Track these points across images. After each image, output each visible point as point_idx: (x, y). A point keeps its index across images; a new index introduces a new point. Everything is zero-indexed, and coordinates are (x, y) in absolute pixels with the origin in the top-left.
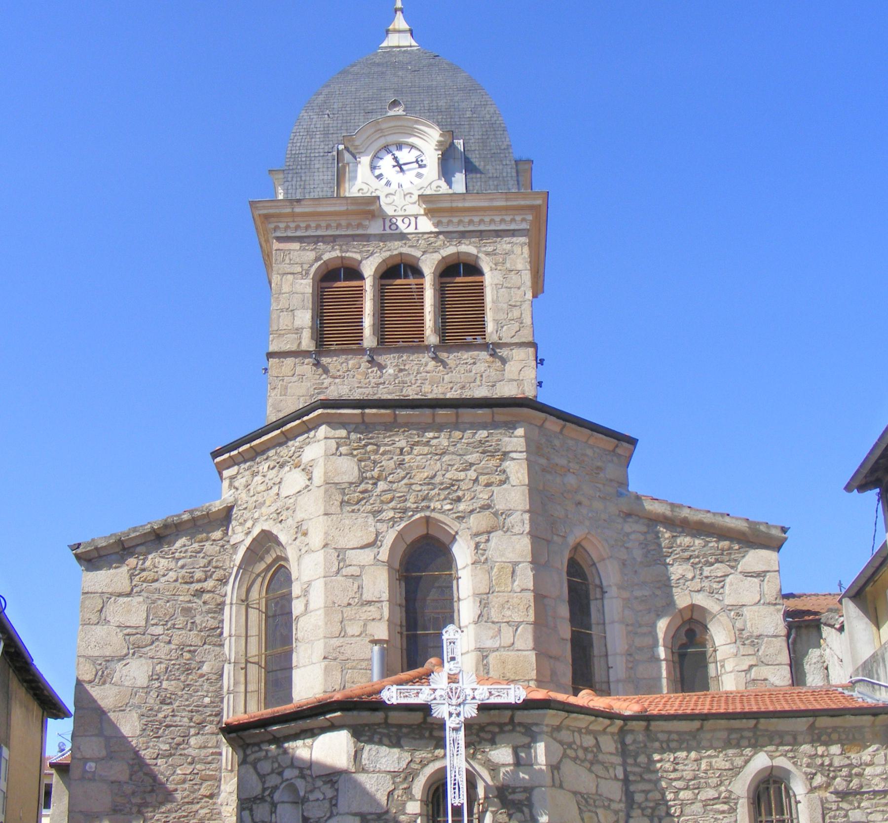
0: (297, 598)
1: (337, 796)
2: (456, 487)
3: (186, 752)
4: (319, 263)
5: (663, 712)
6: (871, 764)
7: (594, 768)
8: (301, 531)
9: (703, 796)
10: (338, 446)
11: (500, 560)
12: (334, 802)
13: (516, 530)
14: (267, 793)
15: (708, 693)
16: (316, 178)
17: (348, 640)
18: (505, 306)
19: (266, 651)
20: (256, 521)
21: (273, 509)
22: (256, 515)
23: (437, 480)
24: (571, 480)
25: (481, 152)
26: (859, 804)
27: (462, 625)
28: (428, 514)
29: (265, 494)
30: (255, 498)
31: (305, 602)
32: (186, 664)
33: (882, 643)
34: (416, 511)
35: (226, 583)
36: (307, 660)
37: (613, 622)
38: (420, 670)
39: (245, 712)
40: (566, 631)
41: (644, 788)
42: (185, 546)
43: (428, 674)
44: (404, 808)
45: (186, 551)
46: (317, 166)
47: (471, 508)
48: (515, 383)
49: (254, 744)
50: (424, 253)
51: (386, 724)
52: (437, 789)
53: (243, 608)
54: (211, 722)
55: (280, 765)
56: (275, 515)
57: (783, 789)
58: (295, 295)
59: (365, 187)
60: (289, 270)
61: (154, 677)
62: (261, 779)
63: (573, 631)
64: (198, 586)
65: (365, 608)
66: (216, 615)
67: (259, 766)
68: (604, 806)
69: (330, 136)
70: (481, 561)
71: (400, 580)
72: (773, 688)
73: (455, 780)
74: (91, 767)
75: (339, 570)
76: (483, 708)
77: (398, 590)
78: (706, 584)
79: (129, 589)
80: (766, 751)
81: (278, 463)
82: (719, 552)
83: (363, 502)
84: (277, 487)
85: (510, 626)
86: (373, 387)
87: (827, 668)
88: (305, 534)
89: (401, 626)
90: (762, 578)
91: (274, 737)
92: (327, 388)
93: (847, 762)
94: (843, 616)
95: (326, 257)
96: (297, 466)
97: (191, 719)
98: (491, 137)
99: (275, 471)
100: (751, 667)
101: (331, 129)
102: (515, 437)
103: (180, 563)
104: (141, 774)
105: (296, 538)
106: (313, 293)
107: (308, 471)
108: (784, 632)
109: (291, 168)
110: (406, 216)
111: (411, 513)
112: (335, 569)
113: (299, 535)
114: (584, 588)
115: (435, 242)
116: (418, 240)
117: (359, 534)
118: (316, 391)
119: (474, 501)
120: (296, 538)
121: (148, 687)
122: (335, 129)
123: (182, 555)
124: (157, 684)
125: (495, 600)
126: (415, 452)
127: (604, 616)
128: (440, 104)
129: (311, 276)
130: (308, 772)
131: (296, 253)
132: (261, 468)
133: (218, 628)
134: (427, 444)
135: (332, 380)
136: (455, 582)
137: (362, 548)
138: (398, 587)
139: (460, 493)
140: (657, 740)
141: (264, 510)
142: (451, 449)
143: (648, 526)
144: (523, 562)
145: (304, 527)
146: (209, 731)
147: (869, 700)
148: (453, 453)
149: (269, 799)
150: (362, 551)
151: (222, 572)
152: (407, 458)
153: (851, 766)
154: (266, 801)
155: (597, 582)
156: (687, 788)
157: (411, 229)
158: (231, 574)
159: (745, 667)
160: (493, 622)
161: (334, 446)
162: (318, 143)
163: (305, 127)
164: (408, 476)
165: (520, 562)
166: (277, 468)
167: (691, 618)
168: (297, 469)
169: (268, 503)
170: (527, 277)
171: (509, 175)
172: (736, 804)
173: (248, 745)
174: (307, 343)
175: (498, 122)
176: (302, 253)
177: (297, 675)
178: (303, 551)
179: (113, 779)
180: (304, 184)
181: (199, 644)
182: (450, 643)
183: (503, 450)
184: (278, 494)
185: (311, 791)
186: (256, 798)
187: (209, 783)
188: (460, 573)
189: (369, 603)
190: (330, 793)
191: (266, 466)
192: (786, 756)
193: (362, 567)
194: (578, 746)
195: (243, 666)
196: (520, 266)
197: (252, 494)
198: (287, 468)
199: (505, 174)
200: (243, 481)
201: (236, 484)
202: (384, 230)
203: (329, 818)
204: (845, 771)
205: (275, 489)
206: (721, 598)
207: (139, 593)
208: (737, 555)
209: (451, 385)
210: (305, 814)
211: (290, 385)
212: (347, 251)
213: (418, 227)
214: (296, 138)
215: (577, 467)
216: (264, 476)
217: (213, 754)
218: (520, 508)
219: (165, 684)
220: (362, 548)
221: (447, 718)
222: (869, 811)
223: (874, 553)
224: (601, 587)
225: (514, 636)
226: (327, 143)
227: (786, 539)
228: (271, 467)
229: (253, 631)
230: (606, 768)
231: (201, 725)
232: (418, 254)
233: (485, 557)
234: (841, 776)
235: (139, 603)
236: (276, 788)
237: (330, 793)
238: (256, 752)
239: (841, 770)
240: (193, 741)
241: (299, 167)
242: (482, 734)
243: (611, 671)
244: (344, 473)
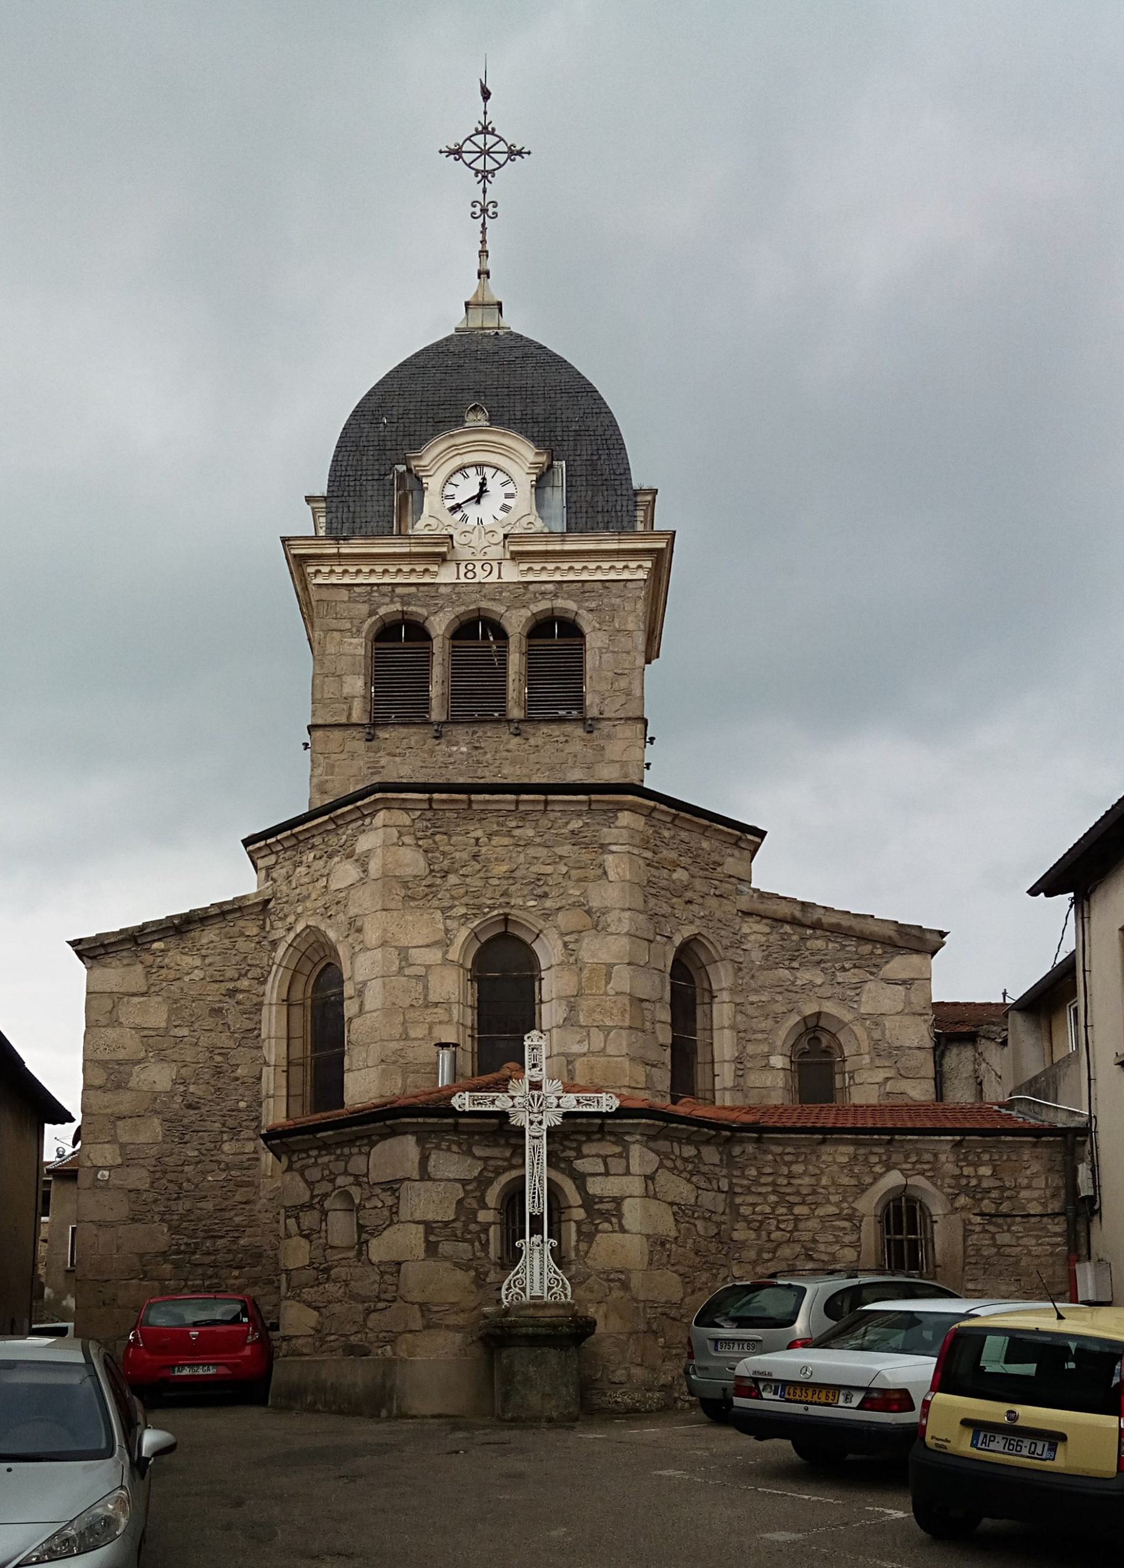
0: (351, 998)
1: (398, 1203)
2: (541, 883)
3: (217, 1158)
4: (374, 618)
5: (778, 1125)
6: (1029, 1187)
7: (694, 1179)
8: (355, 927)
9: (820, 1212)
10: (401, 835)
11: (591, 961)
12: (394, 1210)
13: (611, 929)
14: (316, 1200)
15: (833, 1104)
16: (369, 509)
17: (409, 1043)
18: (610, 674)
19: (312, 1053)
20: (299, 916)
21: (320, 903)
22: (300, 910)
23: (517, 874)
24: (680, 875)
25: (589, 478)
26: (1010, 1226)
27: (544, 1028)
28: (507, 910)
29: (310, 887)
30: (298, 891)
31: (359, 1003)
32: (216, 1067)
33: (1055, 1061)
34: (492, 908)
35: (264, 982)
36: (361, 1063)
37: (723, 1028)
38: (495, 1075)
39: (288, 1116)
40: (665, 1036)
41: (751, 1201)
42: (212, 942)
43: (508, 1079)
44: (476, 1216)
45: (215, 948)
46: (370, 493)
47: (559, 905)
48: (618, 765)
49: (301, 1151)
50: (508, 608)
51: (457, 1124)
52: (513, 1197)
53: (285, 1008)
54: (247, 1128)
55: (331, 1173)
56: (323, 910)
57: (918, 1208)
58: (343, 657)
59: (432, 521)
60: (334, 626)
61: (179, 1081)
62: (309, 1187)
63: (673, 1037)
64: (231, 985)
65: (430, 1011)
66: (252, 1016)
67: (307, 1172)
68: (704, 1218)
69: (388, 453)
70: (571, 959)
71: (471, 980)
72: (910, 1102)
73: (535, 1189)
74: (103, 1176)
75: (401, 968)
76: (567, 1115)
77: (470, 991)
78: (838, 990)
79: (146, 988)
80: (899, 1169)
81: (326, 852)
82: (857, 957)
83: (429, 897)
84: (325, 879)
85: (600, 1030)
86: (440, 767)
87: (980, 1084)
88: (359, 930)
89: (472, 1028)
90: (909, 986)
91: (325, 1143)
92: (383, 767)
93: (998, 1183)
94: (1007, 1030)
95: (382, 611)
96: (349, 857)
97: (224, 1125)
98: (603, 457)
99: (321, 862)
100: (887, 1079)
101: (389, 443)
102: (617, 827)
103: (208, 961)
104: (164, 1181)
105: (348, 935)
106: (365, 656)
107: (363, 863)
108: (928, 1043)
109: (335, 494)
110: (487, 562)
111: (487, 910)
112: (395, 968)
113: (353, 931)
114: (690, 991)
115: (524, 594)
116: (501, 593)
117: (425, 931)
118: (370, 771)
119: (563, 897)
120: (348, 935)
121: (171, 1091)
122: (394, 443)
123: (210, 951)
124: (182, 1088)
125: (585, 1004)
126: (493, 843)
127: (712, 1021)
128: (536, 412)
129: (364, 634)
130: (365, 1179)
131: (343, 606)
132: (304, 858)
133: (255, 1029)
134: (509, 834)
135: (391, 758)
136: (537, 984)
137: (428, 946)
138: (469, 988)
139: (546, 889)
140: (771, 1152)
141: (308, 904)
142: (538, 840)
143: (772, 927)
144: (618, 964)
145: (358, 924)
146: (246, 1137)
147: (1032, 1121)
148: (539, 845)
149: (317, 1206)
150: (428, 950)
151: (259, 970)
152: (484, 850)
153: (1003, 1189)
154: (315, 1208)
155: (706, 986)
156: (803, 1203)
157: (493, 578)
158: (269, 972)
159: (879, 1079)
160: (581, 1027)
161: (396, 834)
162: (371, 462)
163: (352, 439)
164: (485, 869)
165: (615, 964)
166: (324, 858)
167: (817, 1026)
168: (349, 860)
169: (313, 896)
170: (640, 639)
171: (624, 509)
172: (861, 1221)
173: (294, 1152)
174: (358, 714)
175: (614, 437)
176: (352, 605)
177: (348, 1078)
178: (357, 949)
179: (130, 1187)
180: (353, 518)
181: (233, 1046)
182: (533, 1049)
183: (602, 842)
184: (326, 887)
185: (368, 1199)
186: (303, 1206)
187: (246, 1189)
188: (543, 974)
189: (436, 1004)
190: (390, 1201)
191: (312, 855)
192: (923, 1174)
193: (428, 967)
194: (677, 1156)
195: (285, 1069)
196: (631, 626)
197: (294, 885)
198: (336, 859)
199: (619, 508)
200: (284, 871)
201: (274, 875)
202: (458, 578)
203: (389, 1226)
204: (995, 1194)
205: (324, 880)
206: (856, 1006)
207: (157, 994)
208: (879, 960)
209: (538, 766)
210: (360, 1222)
211: (338, 763)
212: (409, 604)
213: (502, 576)
214: (341, 454)
215: (690, 861)
216: (309, 867)
217: (249, 1160)
218: (618, 906)
219: (192, 1088)
220: (428, 946)
221: (527, 1126)
222: (1020, 1235)
223: (1057, 962)
224: (710, 991)
225: (605, 1042)
226: (383, 462)
227: (943, 944)
228: (318, 856)
229: (297, 1032)
230: (708, 1179)
231: (234, 1132)
232: (501, 609)
233: (574, 957)
234: (989, 1198)
235: (159, 1003)
236: (326, 1195)
237: (390, 1201)
238: (303, 1159)
239: (989, 1192)
240: (226, 1147)
241: (346, 494)
242: (566, 1143)
243: (717, 1078)
244: (407, 865)
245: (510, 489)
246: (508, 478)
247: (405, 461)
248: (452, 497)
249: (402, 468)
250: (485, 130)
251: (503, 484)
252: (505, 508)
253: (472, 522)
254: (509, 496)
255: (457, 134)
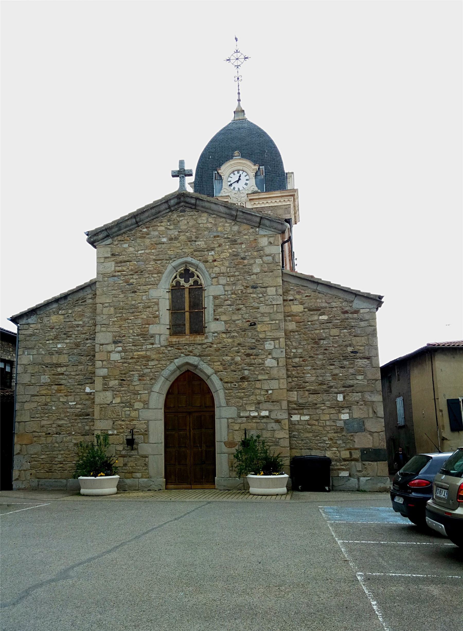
245: (247, 177)
246: (246, 174)
247: (216, 170)
248: (229, 182)
249: (216, 172)
250: (238, 67)
251: (245, 176)
252: (246, 184)
253: (236, 189)
254: (247, 180)
255: (245, 65)
